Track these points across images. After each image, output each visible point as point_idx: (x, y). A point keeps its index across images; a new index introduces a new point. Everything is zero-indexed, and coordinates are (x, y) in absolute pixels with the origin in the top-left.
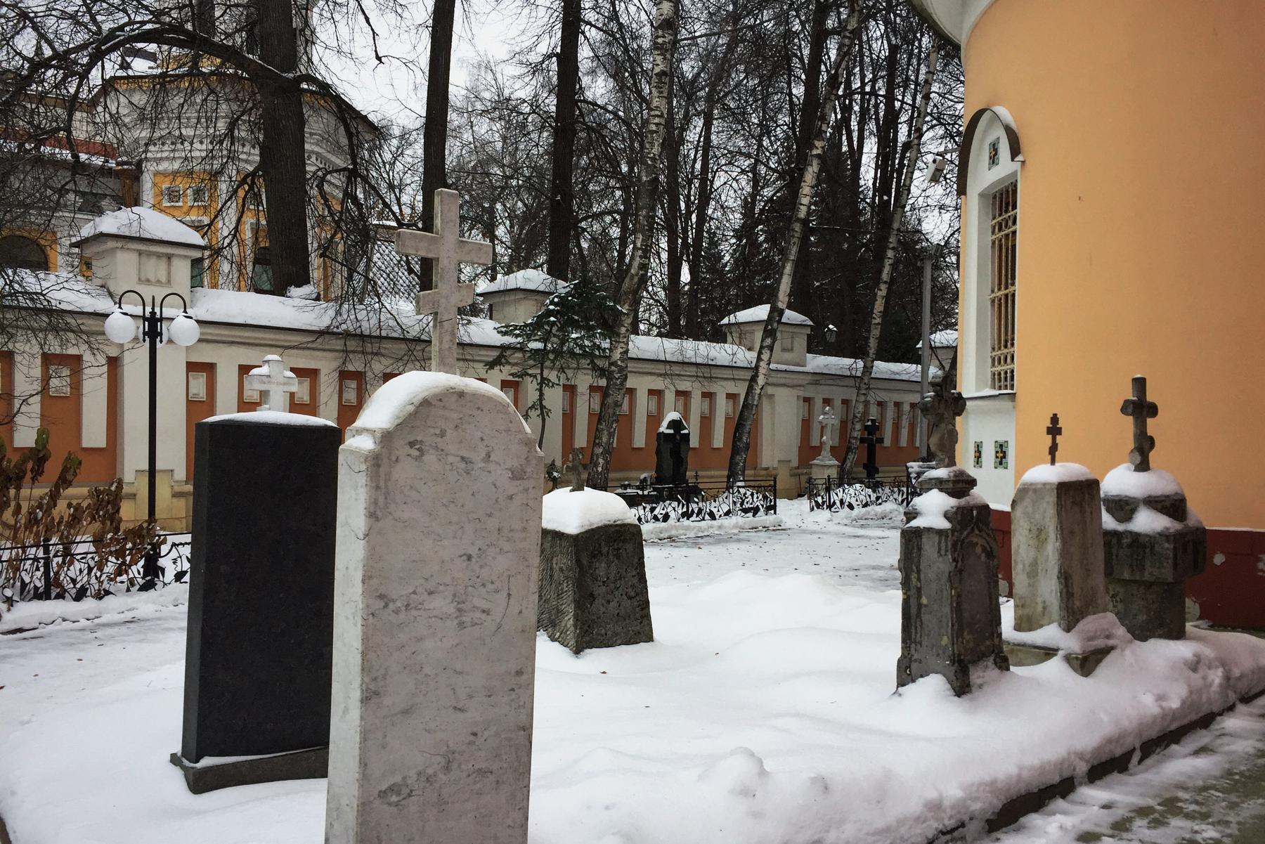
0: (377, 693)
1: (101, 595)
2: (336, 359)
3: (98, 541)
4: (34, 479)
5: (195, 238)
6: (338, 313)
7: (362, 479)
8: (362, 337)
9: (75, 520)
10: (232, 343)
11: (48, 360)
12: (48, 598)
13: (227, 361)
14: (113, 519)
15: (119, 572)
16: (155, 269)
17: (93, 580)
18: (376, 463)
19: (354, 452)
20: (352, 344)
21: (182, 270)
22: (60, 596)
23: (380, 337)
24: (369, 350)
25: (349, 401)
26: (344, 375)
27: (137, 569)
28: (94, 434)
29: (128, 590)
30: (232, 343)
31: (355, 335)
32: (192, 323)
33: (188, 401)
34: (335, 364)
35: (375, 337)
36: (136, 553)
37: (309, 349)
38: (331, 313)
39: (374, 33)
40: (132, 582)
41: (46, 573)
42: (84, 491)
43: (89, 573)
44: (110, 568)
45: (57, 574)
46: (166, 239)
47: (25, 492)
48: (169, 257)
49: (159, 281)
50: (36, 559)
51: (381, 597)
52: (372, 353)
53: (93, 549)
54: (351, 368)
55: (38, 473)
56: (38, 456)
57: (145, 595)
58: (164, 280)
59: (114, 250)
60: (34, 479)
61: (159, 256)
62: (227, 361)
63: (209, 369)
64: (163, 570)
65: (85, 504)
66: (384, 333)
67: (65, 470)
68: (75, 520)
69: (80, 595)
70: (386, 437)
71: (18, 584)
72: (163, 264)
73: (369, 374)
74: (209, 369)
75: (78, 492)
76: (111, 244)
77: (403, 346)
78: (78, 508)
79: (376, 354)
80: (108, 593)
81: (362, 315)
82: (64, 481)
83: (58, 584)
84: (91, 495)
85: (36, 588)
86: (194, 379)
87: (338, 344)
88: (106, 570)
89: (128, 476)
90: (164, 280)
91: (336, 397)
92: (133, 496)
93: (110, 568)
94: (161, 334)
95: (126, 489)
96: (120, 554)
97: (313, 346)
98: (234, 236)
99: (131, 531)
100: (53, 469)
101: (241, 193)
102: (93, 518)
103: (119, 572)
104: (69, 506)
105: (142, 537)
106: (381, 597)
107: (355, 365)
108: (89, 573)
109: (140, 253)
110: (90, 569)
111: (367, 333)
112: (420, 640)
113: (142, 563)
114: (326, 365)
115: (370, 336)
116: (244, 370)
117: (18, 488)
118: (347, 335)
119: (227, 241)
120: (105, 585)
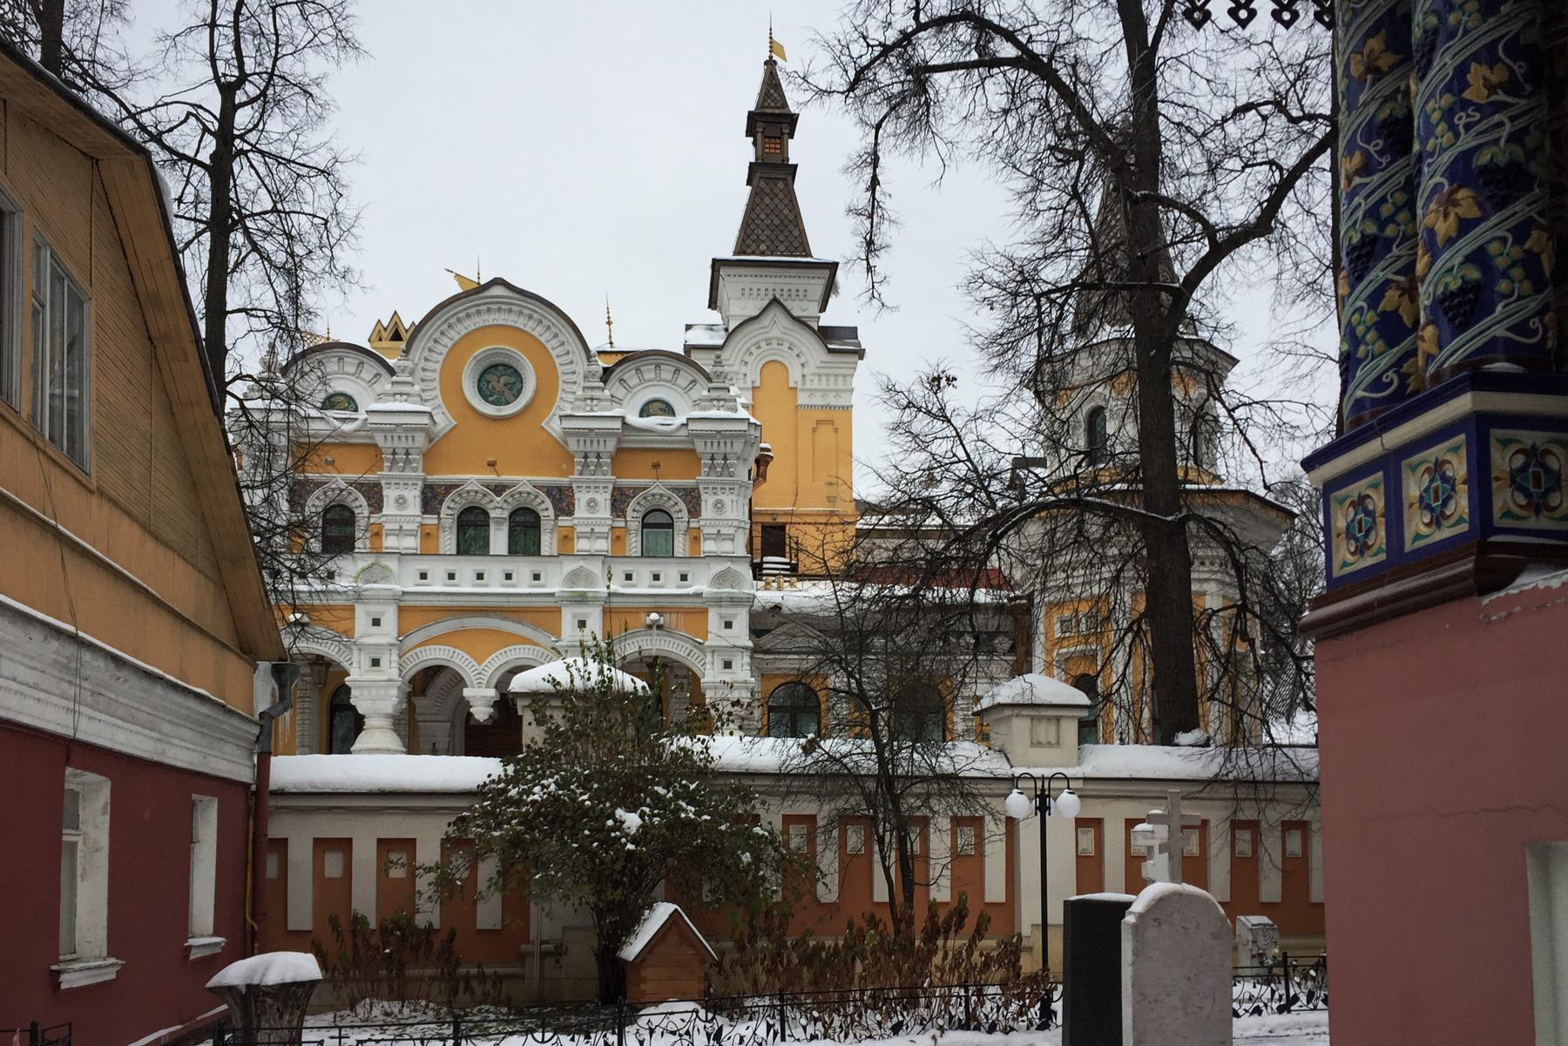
0: (1141, 1042)
1: (1007, 1030)
2: (1226, 808)
3: (1003, 985)
4: (956, 931)
5: (1081, 698)
6: (1228, 759)
7: (1130, 937)
8: (1255, 782)
9: (986, 966)
10: (1119, 797)
11: (957, 821)
12: (969, 1029)
13: (1114, 816)
14: (1015, 966)
15: (1021, 1013)
16: (1046, 731)
17: (1001, 1018)
18: (1135, 928)
19: (1127, 924)
20: (1243, 792)
21: (1070, 730)
22: (977, 1028)
23: (1275, 783)
24: (1262, 796)
25: (1242, 852)
26: (1236, 825)
27: (1035, 1012)
28: (995, 891)
29: (1028, 1028)
30: (1119, 797)
31: (1249, 782)
32: (1074, 797)
33: (1077, 856)
34: (1225, 814)
35: (1268, 782)
36: (1035, 997)
37: (1196, 799)
38: (1220, 759)
39: (1261, 462)
40: (1031, 1023)
41: (967, 1007)
42: (993, 943)
43: (998, 1011)
44: (1014, 1007)
45: (974, 1009)
46: (1055, 702)
47: (950, 943)
48: (1058, 719)
49: (1049, 743)
50: (959, 996)
51: (1142, 994)
52: (1266, 800)
53: (1000, 991)
54: (1241, 816)
55: (960, 926)
56: (959, 914)
57: (1041, 1034)
58: (1053, 740)
59: (1009, 718)
60: (956, 931)
61: (1049, 718)
62: (1114, 816)
63: (1096, 824)
64: (1055, 1013)
65: (995, 954)
66: (1279, 778)
67: (978, 925)
68: (986, 966)
69: (991, 1029)
70: (1141, 916)
71: (947, 1017)
72: (1052, 728)
73: (1264, 825)
74: (1096, 824)
75: (988, 944)
76: (1008, 712)
77: (1302, 790)
78: (988, 957)
79: (1272, 800)
80: (1012, 1029)
81: (1254, 760)
82: (979, 934)
83: (976, 1019)
84: (999, 946)
85: (960, 1020)
86: (1083, 833)
87: (1228, 792)
88: (1011, 1009)
89: (1026, 931)
90: (1053, 740)
91: (1227, 851)
92: (1030, 949)
93: (1014, 1007)
94: (1049, 808)
95: (1025, 943)
96: (1020, 997)
97: (1202, 795)
98: (1123, 681)
99: (1029, 978)
100: (970, 923)
101: (1128, 640)
102: (1000, 966)
103: (1021, 1013)
104: (981, 955)
105: (1037, 983)
106: (1142, 994)
107: (1249, 813)
108: (998, 1011)
109: (1032, 718)
110: (999, 1008)
111: (1260, 778)
112: (1163, 1018)
113: (1038, 1006)
114: (1216, 815)
115: (1264, 782)
116: (1131, 823)
117: (946, 939)
118: (1238, 782)
119: (1115, 687)
120: (1011, 1023)
